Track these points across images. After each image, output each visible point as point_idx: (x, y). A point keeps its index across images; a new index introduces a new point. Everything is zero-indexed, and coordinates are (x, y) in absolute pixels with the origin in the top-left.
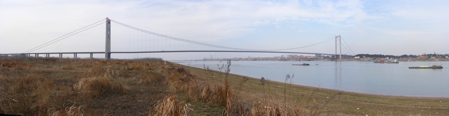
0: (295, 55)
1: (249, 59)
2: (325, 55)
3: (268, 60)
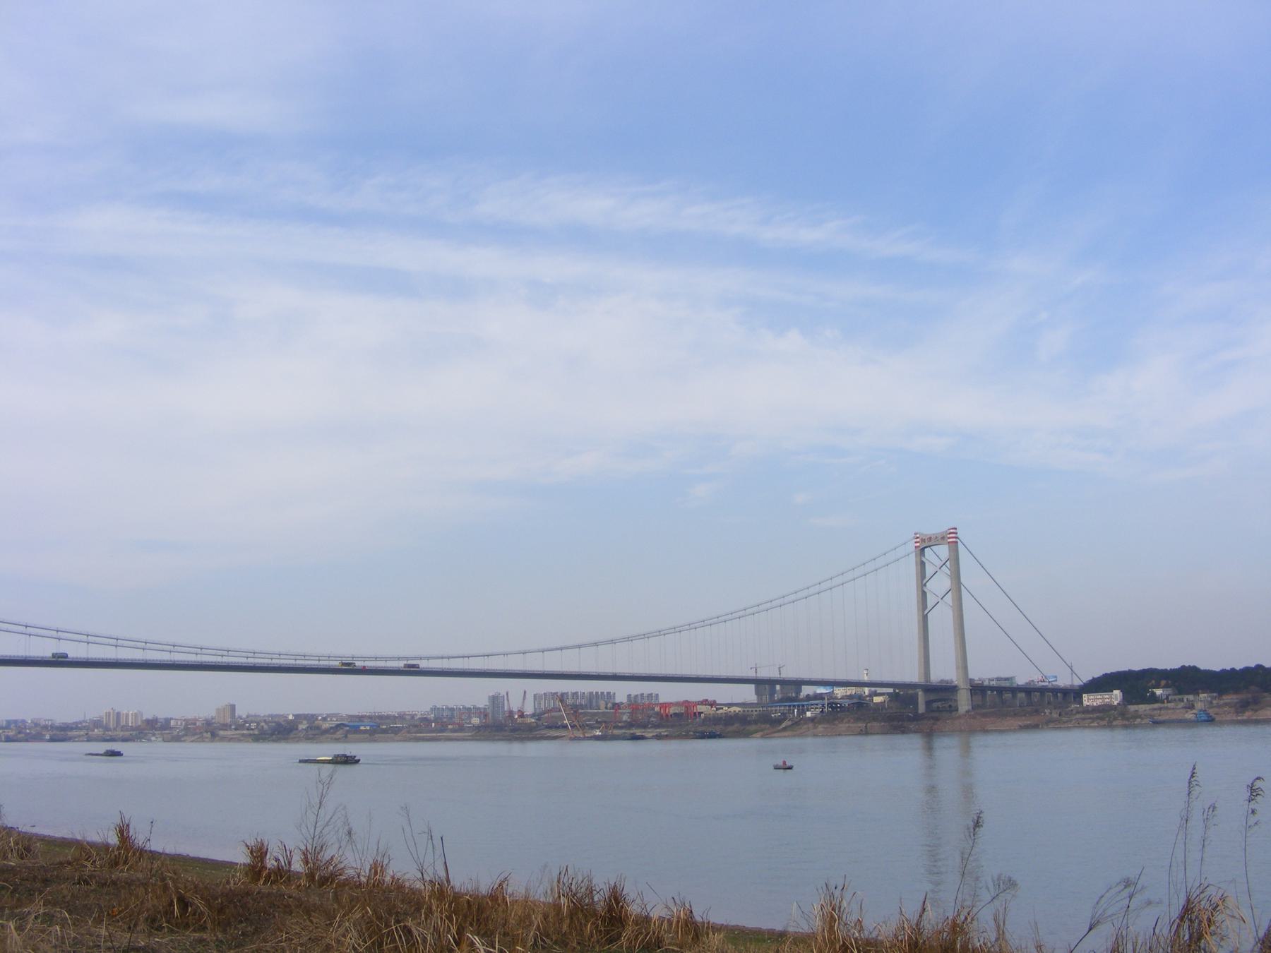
0: (593, 698)
1: (225, 727)
2: (840, 692)
3: (385, 731)
